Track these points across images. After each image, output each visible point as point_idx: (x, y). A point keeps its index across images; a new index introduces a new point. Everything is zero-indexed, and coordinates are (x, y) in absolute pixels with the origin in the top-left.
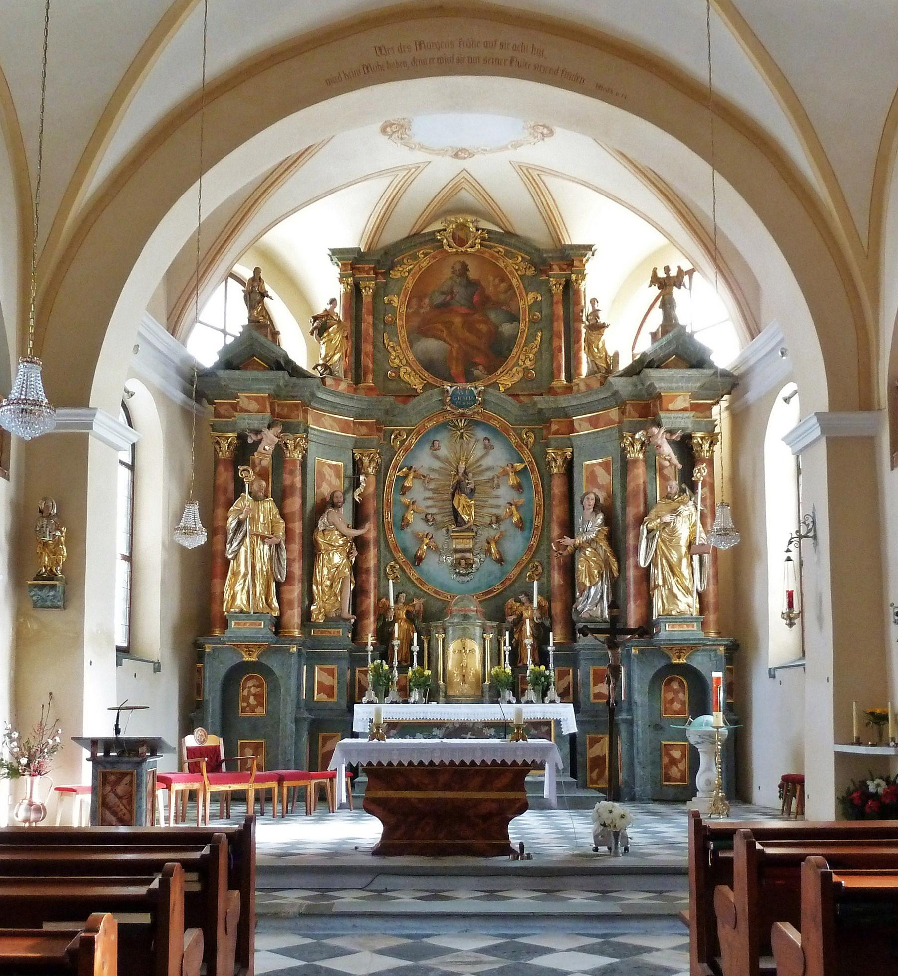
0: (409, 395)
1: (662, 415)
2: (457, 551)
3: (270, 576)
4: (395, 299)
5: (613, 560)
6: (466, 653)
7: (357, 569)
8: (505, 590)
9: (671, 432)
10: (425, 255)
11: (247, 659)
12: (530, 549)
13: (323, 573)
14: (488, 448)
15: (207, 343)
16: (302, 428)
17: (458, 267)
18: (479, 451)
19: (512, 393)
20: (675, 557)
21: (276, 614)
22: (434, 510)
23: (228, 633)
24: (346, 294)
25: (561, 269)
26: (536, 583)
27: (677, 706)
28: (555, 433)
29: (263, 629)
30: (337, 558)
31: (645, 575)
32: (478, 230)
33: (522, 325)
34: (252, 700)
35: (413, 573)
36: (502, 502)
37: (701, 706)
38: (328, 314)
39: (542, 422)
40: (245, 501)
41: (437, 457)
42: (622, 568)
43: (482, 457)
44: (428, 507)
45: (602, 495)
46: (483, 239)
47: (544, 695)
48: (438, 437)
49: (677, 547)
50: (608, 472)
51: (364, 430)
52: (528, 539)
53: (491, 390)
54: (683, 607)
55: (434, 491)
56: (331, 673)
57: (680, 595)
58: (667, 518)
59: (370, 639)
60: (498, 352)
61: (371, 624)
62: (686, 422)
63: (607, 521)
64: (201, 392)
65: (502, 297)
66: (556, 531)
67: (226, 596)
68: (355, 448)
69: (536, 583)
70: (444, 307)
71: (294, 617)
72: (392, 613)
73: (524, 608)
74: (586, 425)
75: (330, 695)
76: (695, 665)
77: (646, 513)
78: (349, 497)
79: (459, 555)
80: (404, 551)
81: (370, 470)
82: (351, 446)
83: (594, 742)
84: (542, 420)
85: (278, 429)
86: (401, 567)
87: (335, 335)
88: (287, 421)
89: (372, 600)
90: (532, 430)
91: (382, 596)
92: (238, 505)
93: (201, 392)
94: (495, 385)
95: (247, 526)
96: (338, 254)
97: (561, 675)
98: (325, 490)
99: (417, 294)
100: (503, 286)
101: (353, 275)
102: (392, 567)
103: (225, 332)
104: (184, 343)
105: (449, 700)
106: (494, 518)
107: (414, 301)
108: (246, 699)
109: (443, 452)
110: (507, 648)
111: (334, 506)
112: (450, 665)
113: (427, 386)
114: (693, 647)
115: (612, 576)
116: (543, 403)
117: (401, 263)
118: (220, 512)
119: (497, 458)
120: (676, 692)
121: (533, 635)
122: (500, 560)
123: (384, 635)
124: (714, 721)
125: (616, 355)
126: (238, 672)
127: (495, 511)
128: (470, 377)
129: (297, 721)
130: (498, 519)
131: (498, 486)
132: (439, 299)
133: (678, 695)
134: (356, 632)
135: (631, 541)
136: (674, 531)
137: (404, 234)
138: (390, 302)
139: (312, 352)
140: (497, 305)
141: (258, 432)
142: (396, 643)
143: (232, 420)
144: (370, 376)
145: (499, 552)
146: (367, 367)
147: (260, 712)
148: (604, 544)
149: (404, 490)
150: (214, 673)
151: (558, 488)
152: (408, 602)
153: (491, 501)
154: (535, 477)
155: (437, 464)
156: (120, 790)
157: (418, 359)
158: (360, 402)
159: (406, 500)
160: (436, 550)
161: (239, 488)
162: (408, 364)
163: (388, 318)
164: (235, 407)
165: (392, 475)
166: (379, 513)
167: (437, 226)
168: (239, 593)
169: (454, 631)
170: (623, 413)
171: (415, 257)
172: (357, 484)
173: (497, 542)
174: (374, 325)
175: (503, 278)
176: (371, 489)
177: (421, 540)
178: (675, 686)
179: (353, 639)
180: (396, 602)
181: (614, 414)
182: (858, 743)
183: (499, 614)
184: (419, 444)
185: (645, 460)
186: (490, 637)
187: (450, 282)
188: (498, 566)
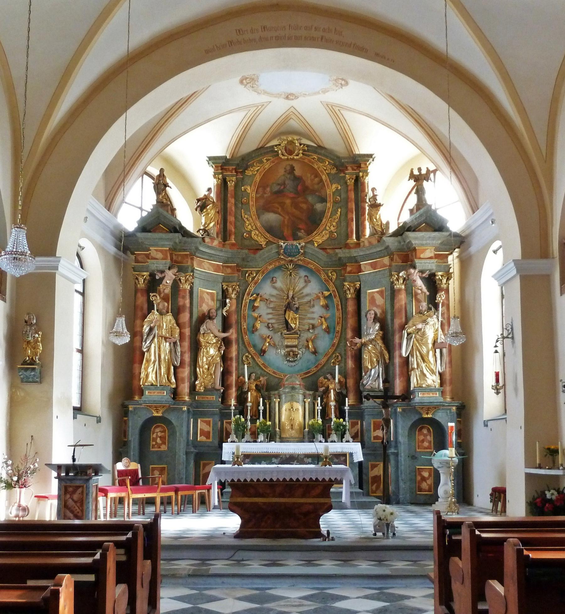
0: (258, 248)
1: (417, 261)
2: (287, 346)
3: (170, 362)
4: (249, 188)
5: (385, 352)
6: (293, 411)
7: (225, 358)
8: (318, 371)
9: (422, 272)
10: (267, 160)
11: (155, 414)
12: (333, 345)
13: (203, 360)
14: (307, 282)
15: (130, 215)
16: (190, 269)
17: (288, 168)
18: (301, 284)
19: (322, 247)
20: (424, 350)
21: (174, 386)
22: (273, 321)
23: (143, 398)
24: (217, 185)
25: (353, 169)
26: (337, 367)
27: (426, 444)
28: (349, 273)
29: (165, 395)
30: (212, 351)
31: (406, 362)
32: (301, 145)
33: (328, 205)
34: (159, 440)
35: (260, 361)
36: (316, 316)
37: (441, 444)
38: (206, 198)
39: (341, 266)
40: (154, 315)
41: (275, 288)
42: (391, 357)
43: (304, 288)
44: (269, 319)
45: (379, 312)
46: (304, 151)
47: (343, 437)
48: (276, 275)
49: (426, 344)
50: (383, 297)
51: (229, 270)
52: (332, 339)
53: (309, 246)
54: (429, 382)
55: (273, 309)
56: (208, 423)
57: (428, 375)
58: (420, 326)
59: (233, 402)
60: (313, 221)
61: (233, 392)
62: (432, 265)
63: (382, 328)
64: (126, 246)
65: (316, 187)
66: (350, 334)
67: (142, 375)
68: (223, 282)
69: (337, 367)
70: (279, 193)
71: (185, 388)
72: (246, 386)
73: (329, 383)
74: (369, 267)
75: (208, 437)
76: (437, 418)
77: (406, 323)
78: (220, 313)
79: (289, 349)
80: (254, 346)
81: (233, 296)
82: (221, 280)
83: (374, 467)
84: (341, 264)
85: (175, 270)
86: (252, 357)
87: (211, 211)
88: (180, 265)
89: (234, 377)
90: (334, 271)
91: (240, 375)
92: (150, 317)
93: (126, 246)
94: (312, 242)
95: (156, 331)
96: (212, 160)
97: (353, 425)
98: (205, 308)
99: (263, 185)
100: (317, 180)
101: (222, 173)
102: (247, 357)
103: (141, 209)
104: (116, 216)
105: (282, 440)
106: (311, 326)
107: (261, 190)
108: (155, 440)
109: (279, 284)
110: (319, 408)
111: (210, 318)
112: (283, 419)
113: (269, 243)
114: (436, 407)
115: (385, 362)
116: (342, 253)
117: (252, 166)
118: (138, 322)
119: (313, 288)
120: (425, 435)
121: (335, 400)
122: (315, 353)
123: (241, 400)
124: (450, 454)
125: (388, 223)
126: (150, 423)
127: (312, 322)
128: (295, 237)
129: (187, 453)
130: (314, 327)
131: (313, 306)
132: (276, 188)
133: (427, 437)
134: (224, 397)
135: (397, 340)
136: (424, 334)
137: (254, 147)
138: (245, 190)
139: (196, 222)
140: (313, 192)
141: (162, 272)
142: (249, 404)
143: (146, 264)
144: (233, 237)
145: (314, 347)
146: (231, 231)
147: (164, 448)
148: (380, 342)
149: (254, 308)
150: (135, 424)
151: (351, 307)
152: (257, 379)
153: (309, 315)
154: (336, 300)
155: (275, 292)
156: (76, 497)
157: (263, 226)
158: (226, 253)
159: (255, 314)
160: (275, 346)
161: (151, 307)
162: (256, 229)
163: (244, 200)
164: (148, 256)
165: (247, 299)
166: (239, 323)
167: (275, 142)
168: (150, 373)
169: (286, 397)
170: (392, 259)
171: (261, 162)
172: (224, 304)
173: (312, 341)
174: (236, 205)
175: (317, 175)
176: (234, 308)
177: (265, 340)
178: (425, 431)
179: (222, 402)
180: (249, 379)
181: (386, 260)
182: (540, 467)
183: (314, 386)
184: (264, 279)
185: (406, 289)
186: (308, 400)
187: (283, 178)
188: (313, 356)
